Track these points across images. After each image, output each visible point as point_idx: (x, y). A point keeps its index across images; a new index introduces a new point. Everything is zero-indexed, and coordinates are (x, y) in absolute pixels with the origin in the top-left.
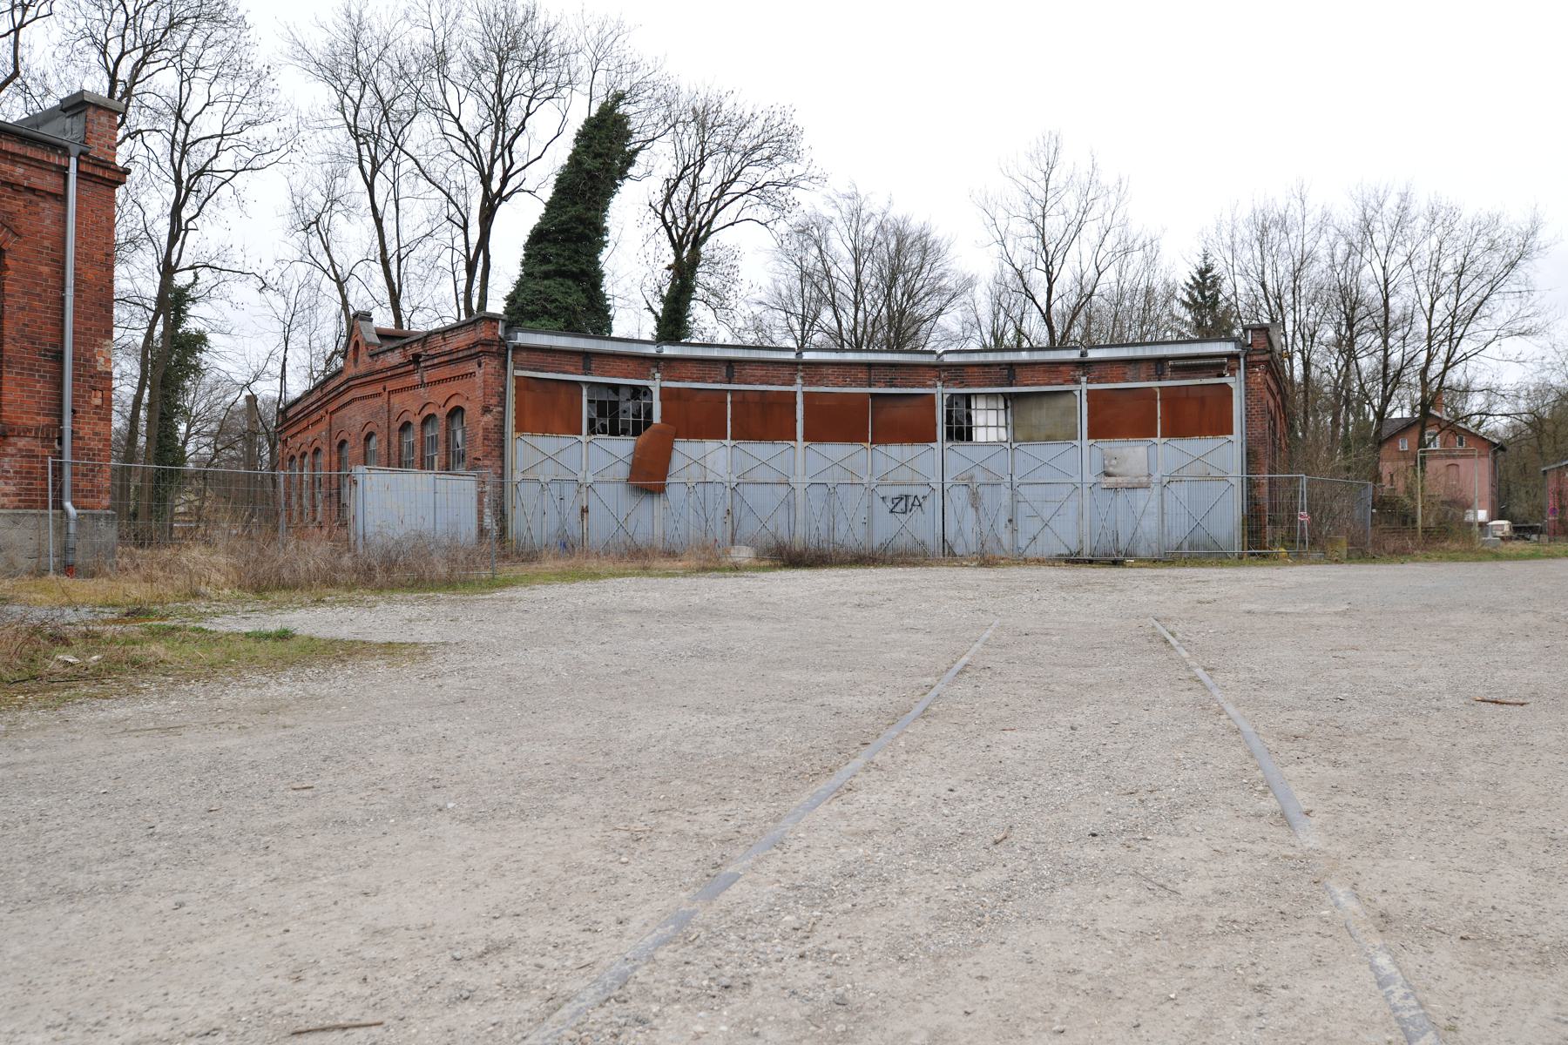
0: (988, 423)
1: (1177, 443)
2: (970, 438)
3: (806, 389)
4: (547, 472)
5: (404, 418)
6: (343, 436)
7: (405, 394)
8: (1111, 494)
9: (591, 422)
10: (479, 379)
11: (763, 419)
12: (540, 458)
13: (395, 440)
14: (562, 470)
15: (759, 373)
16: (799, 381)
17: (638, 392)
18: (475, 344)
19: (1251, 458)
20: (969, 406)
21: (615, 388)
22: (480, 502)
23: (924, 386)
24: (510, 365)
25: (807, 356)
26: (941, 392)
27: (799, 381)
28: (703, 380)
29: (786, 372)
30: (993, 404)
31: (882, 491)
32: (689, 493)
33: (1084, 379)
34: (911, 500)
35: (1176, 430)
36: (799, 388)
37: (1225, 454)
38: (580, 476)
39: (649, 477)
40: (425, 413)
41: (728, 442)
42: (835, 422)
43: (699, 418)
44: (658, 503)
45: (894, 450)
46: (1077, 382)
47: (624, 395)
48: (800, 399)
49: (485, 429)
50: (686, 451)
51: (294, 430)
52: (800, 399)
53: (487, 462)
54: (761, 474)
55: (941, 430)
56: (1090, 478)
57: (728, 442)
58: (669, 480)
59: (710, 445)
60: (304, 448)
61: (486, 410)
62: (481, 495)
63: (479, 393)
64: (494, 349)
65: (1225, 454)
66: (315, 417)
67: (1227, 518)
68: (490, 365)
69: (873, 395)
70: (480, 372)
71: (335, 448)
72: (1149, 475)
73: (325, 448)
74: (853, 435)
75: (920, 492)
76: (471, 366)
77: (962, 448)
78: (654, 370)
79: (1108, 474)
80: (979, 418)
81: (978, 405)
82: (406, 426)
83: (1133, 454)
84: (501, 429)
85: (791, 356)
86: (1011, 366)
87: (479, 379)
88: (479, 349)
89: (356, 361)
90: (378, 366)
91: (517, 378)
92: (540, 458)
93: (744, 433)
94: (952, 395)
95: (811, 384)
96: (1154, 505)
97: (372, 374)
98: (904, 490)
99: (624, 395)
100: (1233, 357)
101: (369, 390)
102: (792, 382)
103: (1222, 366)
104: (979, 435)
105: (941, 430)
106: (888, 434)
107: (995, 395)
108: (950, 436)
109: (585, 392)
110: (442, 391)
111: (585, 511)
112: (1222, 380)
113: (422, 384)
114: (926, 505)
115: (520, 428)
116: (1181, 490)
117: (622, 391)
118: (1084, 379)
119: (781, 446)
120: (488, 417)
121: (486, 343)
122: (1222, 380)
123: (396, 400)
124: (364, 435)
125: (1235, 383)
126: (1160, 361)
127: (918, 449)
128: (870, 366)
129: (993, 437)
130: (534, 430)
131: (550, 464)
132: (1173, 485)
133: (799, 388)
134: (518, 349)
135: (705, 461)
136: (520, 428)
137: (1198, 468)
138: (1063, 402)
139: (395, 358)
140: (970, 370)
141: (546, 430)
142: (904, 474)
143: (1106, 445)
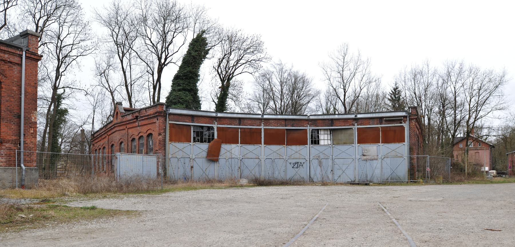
0: (325, 139)
1: (387, 145)
2: (318, 144)
3: (265, 127)
4: (180, 155)
5: (133, 137)
6: (113, 143)
7: (133, 129)
8: (365, 162)
9: (194, 138)
10: (157, 124)
11: (251, 137)
12: (177, 150)
13: (130, 144)
14: (184, 154)
15: (249, 122)
16: (262, 125)
17: (210, 128)
18: (156, 113)
19: (411, 150)
20: (318, 133)
21: (202, 127)
22: (158, 164)
23: (304, 126)
24: (168, 119)
25: (265, 117)
26: (309, 128)
27: (262, 125)
28: (231, 124)
29: (258, 122)
30: (326, 132)
31: (290, 161)
32: (226, 161)
33: (356, 124)
34: (299, 164)
35: (386, 141)
36: (262, 127)
37: (402, 149)
38: (191, 156)
39: (213, 156)
40: (140, 135)
41: (239, 145)
42: (274, 138)
43: (230, 137)
44: (216, 165)
45: (294, 147)
46: (354, 125)
47: (205, 129)
48: (263, 131)
49: (159, 141)
50: (225, 148)
51: (97, 141)
52: (263, 131)
53: (160, 151)
54: (250, 155)
55: (309, 141)
56: (358, 157)
57: (239, 145)
58: (220, 157)
59: (233, 146)
60: (100, 147)
61: (160, 134)
62: (158, 162)
63: (157, 129)
64: (162, 114)
65: (402, 149)
66: (103, 137)
67: (403, 170)
68: (161, 119)
69: (287, 129)
70: (158, 122)
71: (110, 147)
72: (378, 156)
73: (107, 147)
74: (280, 142)
75: (302, 161)
76: (155, 120)
77: (316, 147)
78: (215, 121)
79: (364, 155)
80: (321, 137)
81: (321, 133)
82: (133, 140)
83: (372, 149)
84: (165, 140)
85: (260, 117)
86: (332, 120)
87: (157, 124)
88: (157, 114)
89: (117, 118)
90: (124, 120)
91: (170, 124)
92: (177, 150)
93: (244, 142)
94: (313, 129)
95: (266, 126)
96: (379, 165)
97: (122, 122)
98: (297, 161)
99: (205, 129)
100: (405, 117)
101: (121, 128)
102: (260, 125)
103: (401, 120)
104: (322, 142)
105: (309, 141)
106: (291, 142)
107: (327, 129)
108: (312, 143)
109: (192, 128)
110: (145, 128)
111: (192, 167)
112: (401, 125)
113: (139, 126)
114: (304, 165)
115: (171, 140)
116: (388, 161)
117: (204, 128)
118: (356, 124)
119: (256, 146)
120: (160, 137)
121: (160, 112)
122: (401, 125)
123: (130, 131)
124: (119, 142)
125: (406, 125)
126: (381, 118)
127: (302, 147)
128: (286, 120)
129: (326, 143)
130: (175, 141)
131: (180, 152)
132: (385, 159)
133: (262, 127)
134: (170, 114)
135: (231, 151)
136: (171, 140)
137: (394, 153)
138: (349, 132)
139: (130, 117)
140: (318, 121)
141: (179, 141)
142: (297, 155)
143: (363, 146)
